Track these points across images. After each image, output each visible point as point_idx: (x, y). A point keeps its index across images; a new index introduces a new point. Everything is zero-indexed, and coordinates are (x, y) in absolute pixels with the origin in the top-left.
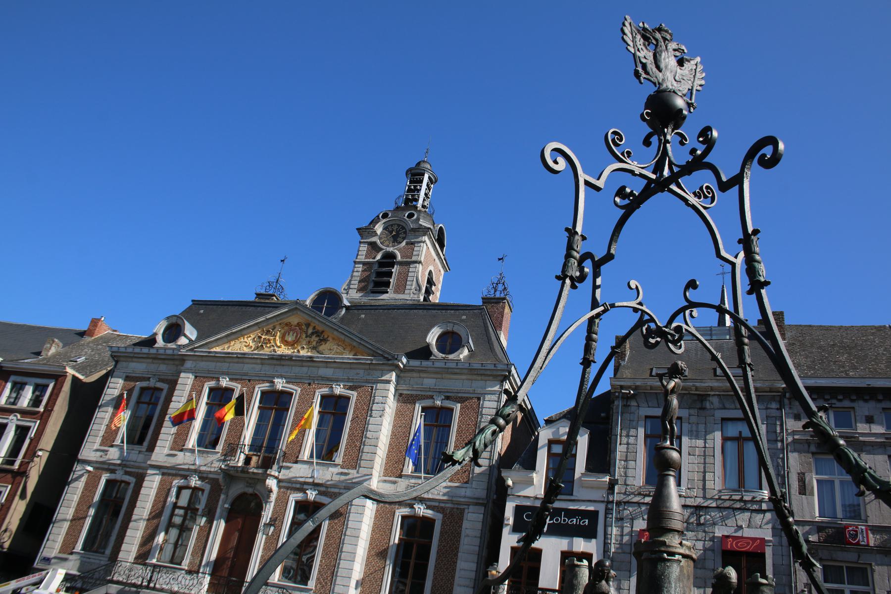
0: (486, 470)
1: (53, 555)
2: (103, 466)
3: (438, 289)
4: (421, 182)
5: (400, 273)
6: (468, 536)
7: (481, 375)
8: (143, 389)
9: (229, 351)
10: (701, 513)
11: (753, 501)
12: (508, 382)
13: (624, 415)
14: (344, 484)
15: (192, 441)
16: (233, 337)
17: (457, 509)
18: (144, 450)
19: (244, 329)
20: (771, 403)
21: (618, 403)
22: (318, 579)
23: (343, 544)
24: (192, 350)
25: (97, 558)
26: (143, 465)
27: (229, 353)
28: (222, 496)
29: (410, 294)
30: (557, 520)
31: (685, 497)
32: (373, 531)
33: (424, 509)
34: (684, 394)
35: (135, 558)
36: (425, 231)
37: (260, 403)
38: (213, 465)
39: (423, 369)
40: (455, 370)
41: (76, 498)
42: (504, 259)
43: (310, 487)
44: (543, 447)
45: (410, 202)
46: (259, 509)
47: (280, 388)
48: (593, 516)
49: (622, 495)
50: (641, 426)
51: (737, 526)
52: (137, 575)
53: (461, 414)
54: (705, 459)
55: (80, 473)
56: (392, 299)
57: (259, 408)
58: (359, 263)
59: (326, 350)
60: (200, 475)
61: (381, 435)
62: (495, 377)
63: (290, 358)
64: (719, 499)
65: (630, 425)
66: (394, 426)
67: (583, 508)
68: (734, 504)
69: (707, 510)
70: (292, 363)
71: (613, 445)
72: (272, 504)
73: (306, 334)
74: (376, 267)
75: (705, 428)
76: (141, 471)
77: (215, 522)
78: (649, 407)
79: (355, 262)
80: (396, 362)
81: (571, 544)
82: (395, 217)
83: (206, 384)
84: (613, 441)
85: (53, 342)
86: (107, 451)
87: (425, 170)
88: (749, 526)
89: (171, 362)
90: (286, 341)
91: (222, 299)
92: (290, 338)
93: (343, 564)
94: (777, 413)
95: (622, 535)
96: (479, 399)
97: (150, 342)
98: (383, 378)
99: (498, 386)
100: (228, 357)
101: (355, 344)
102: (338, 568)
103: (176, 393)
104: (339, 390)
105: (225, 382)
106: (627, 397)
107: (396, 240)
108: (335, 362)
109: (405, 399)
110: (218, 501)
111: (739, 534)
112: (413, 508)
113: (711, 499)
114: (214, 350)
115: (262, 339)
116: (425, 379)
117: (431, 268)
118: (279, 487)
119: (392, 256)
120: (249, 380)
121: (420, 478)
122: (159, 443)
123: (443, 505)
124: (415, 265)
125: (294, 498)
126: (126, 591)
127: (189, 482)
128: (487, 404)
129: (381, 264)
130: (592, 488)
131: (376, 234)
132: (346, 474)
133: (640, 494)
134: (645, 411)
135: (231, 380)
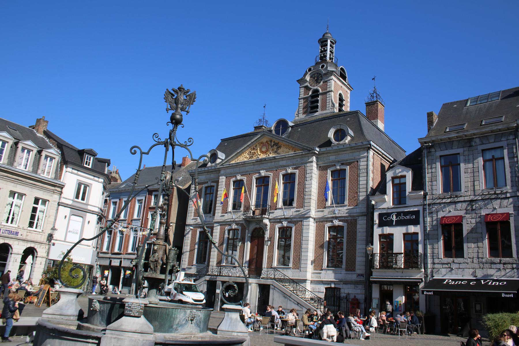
0: (365, 198)
1: (186, 267)
2: (196, 226)
3: (347, 102)
4: (327, 45)
5: (322, 99)
6: (360, 232)
7: (357, 149)
8: (206, 188)
9: (238, 162)
10: (473, 204)
11: (502, 193)
12: (371, 150)
13: (429, 157)
14: (298, 216)
15: (230, 208)
16: (239, 155)
17: (354, 219)
18: (212, 215)
19: (243, 149)
20: (510, 136)
21: (425, 152)
22: (293, 262)
23: (302, 244)
24: (222, 165)
25: (338, 270)
26: (212, 222)
27: (238, 163)
28: (247, 231)
29: (329, 109)
30: (399, 218)
31: (464, 196)
32: (316, 236)
33: (338, 222)
34: (460, 140)
35: (217, 264)
36: (331, 73)
37: (256, 184)
38: (241, 217)
39: (328, 152)
40: (343, 149)
41: (189, 242)
42: (375, 79)
43: (284, 220)
44: (389, 181)
45: (323, 58)
46: (264, 234)
47: (264, 175)
48: (417, 213)
49: (431, 200)
50: (438, 162)
51: (493, 208)
52: (215, 271)
53: (350, 171)
54: (474, 174)
55: (188, 230)
56: (321, 114)
57: (256, 186)
58: (301, 99)
59: (281, 152)
60: (236, 223)
61: (312, 189)
62: (364, 148)
63: (265, 160)
64: (483, 194)
65: (432, 162)
66: (319, 183)
67: (412, 210)
68: (491, 196)
69: (477, 201)
70: (267, 162)
71: (424, 175)
72: (269, 231)
73: (271, 146)
74: (310, 99)
75: (473, 157)
76: (212, 225)
77: (246, 243)
78: (441, 151)
79: (299, 99)
80: (313, 151)
81: (407, 229)
82: (315, 69)
83: (231, 180)
84: (424, 172)
85: (167, 173)
86: (197, 219)
87: (327, 38)
88: (500, 207)
89: (215, 172)
90: (262, 151)
91: (234, 136)
92: (264, 150)
93: (303, 254)
94: (513, 141)
95: (432, 221)
96: (358, 162)
97: (205, 165)
98: (309, 160)
99: (366, 153)
100: (238, 165)
101: (294, 146)
102: (301, 256)
103: (219, 187)
104: (290, 171)
105: (239, 177)
106: (429, 148)
107: (317, 82)
108: (285, 157)
109: (322, 168)
110: (245, 234)
111: (495, 212)
112: (333, 222)
113: (478, 195)
114: (232, 163)
115: (252, 153)
116: (330, 157)
117: (340, 92)
118: (270, 222)
119: (317, 91)
120: (249, 174)
121: (333, 207)
122: (216, 211)
123: (346, 219)
124: (329, 93)
125: (278, 226)
126: (212, 278)
127: (232, 227)
128: (362, 164)
129: (312, 97)
130: (415, 199)
131: (307, 81)
132: (299, 211)
133: (440, 198)
134: (440, 153)
135: (242, 175)
